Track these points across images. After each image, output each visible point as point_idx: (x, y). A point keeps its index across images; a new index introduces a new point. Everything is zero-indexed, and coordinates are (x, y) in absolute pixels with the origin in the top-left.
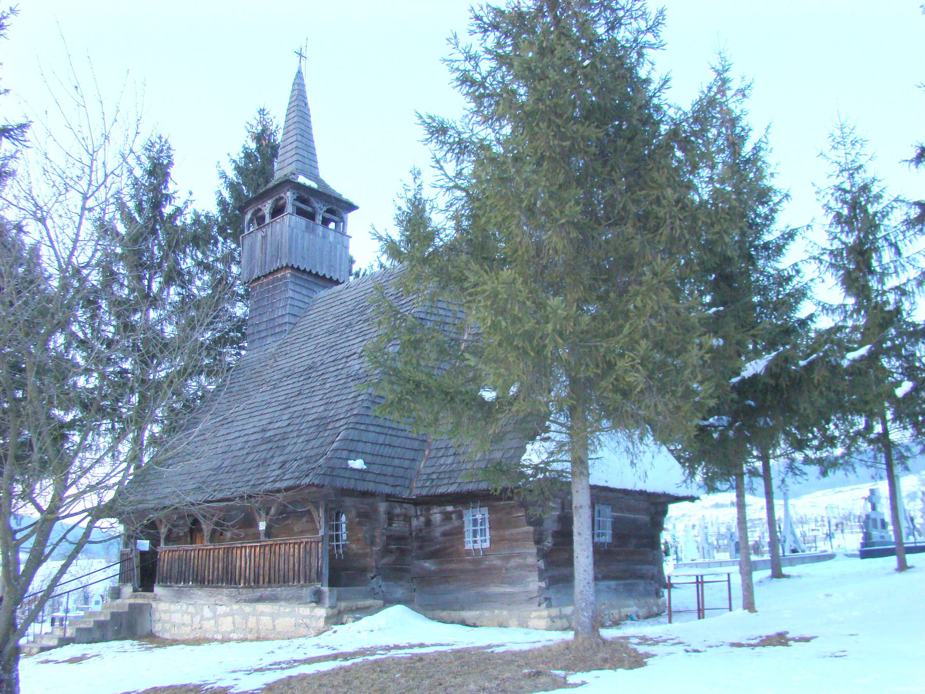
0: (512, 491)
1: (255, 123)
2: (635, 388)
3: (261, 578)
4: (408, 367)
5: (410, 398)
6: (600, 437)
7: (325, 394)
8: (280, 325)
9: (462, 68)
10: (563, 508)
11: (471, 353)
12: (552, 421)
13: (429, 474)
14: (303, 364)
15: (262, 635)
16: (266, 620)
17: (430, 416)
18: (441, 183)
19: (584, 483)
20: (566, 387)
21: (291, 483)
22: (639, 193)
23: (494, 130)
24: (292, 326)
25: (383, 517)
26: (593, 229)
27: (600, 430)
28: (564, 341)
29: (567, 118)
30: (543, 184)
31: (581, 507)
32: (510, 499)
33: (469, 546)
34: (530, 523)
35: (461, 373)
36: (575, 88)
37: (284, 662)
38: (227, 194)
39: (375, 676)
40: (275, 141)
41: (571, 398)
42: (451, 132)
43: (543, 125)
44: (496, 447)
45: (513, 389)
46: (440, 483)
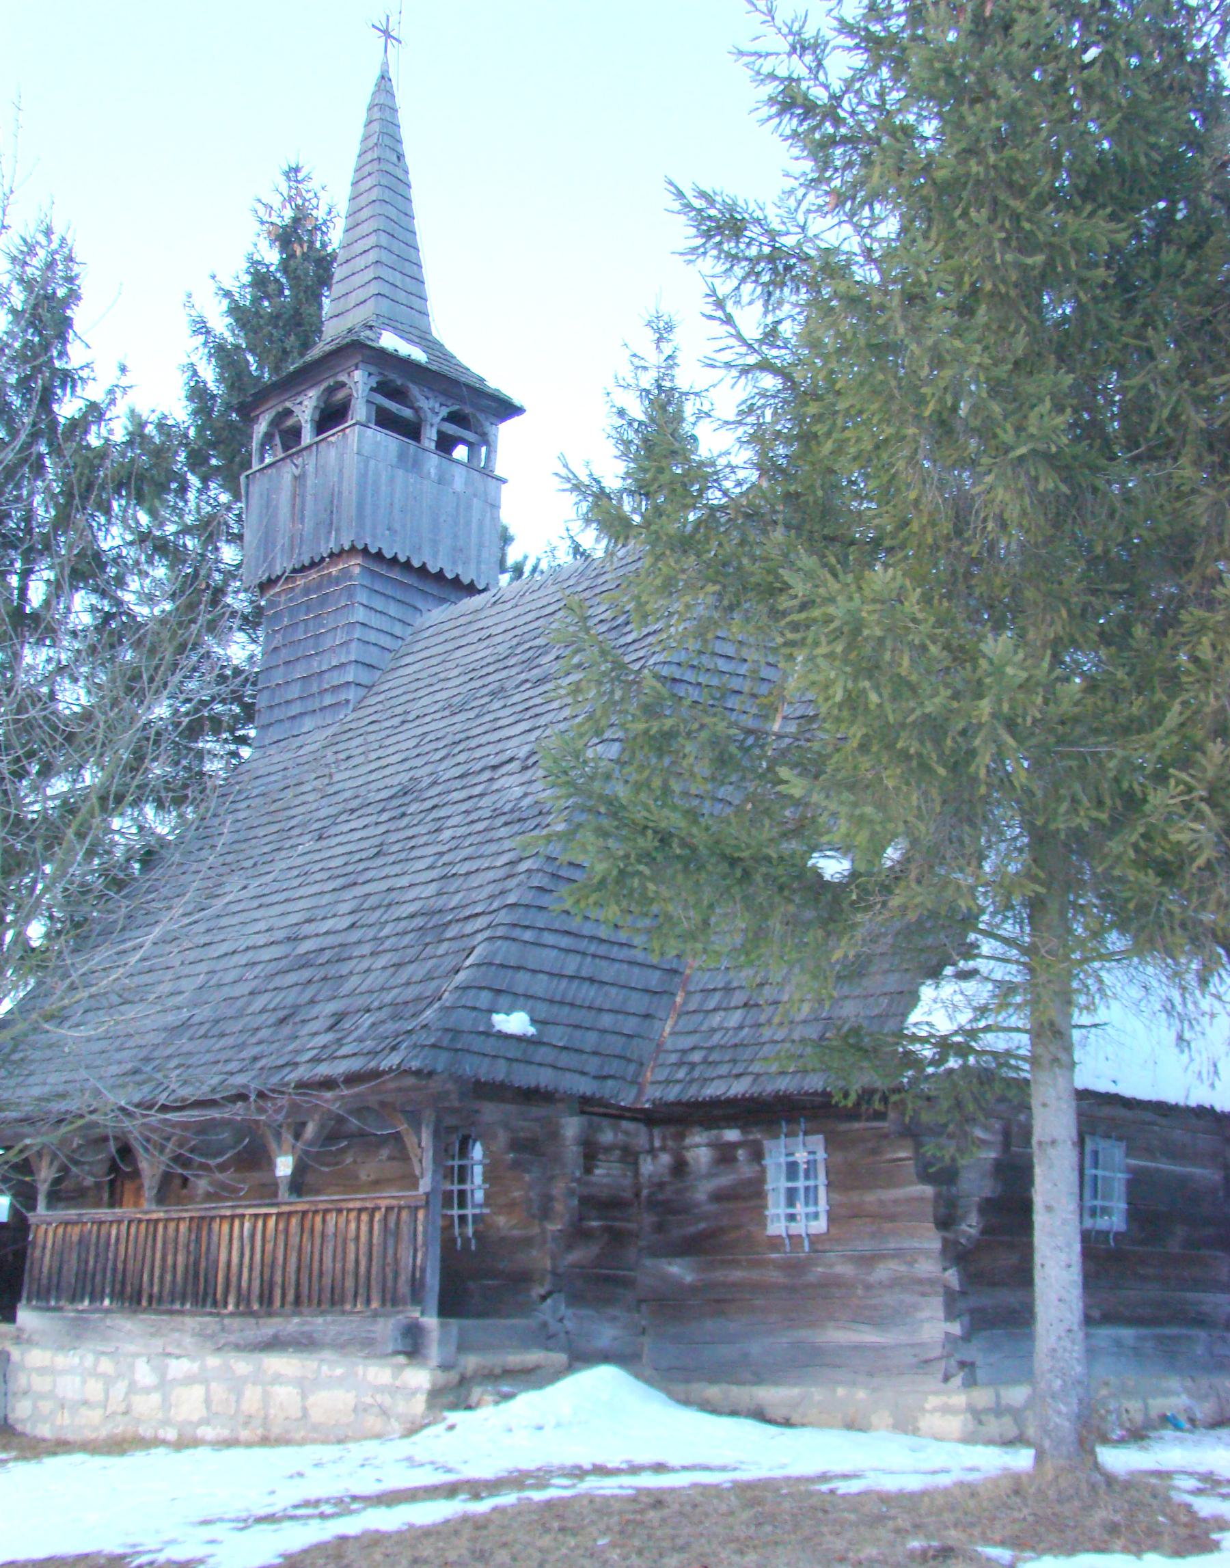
0: (885, 1099)
1: (276, 202)
2: (1192, 859)
3: (278, 1292)
4: (643, 796)
5: (647, 871)
6: (1103, 974)
7: (441, 854)
8: (336, 688)
9: (782, 72)
10: (1006, 1144)
11: (793, 766)
12: (981, 932)
13: (684, 1052)
14: (388, 781)
15: (276, 1431)
16: (285, 1395)
17: (692, 913)
18: (727, 356)
19: (1061, 1082)
20: (1020, 850)
21: (355, 1065)
22: (1212, 381)
23: (858, 228)
24: (362, 692)
25: (572, 1152)
26: (1095, 469)
27: (1101, 957)
28: (1020, 741)
29: (1040, 195)
30: (976, 360)
31: (1053, 1142)
32: (880, 1116)
33: (777, 1228)
34: (925, 1176)
35: (767, 812)
36: (1061, 121)
37: (327, 1501)
38: (209, 374)
39: (546, 1541)
40: (324, 245)
41: (1034, 879)
42: (753, 231)
43: (979, 216)
44: (846, 990)
45: (892, 854)
46: (711, 1072)
